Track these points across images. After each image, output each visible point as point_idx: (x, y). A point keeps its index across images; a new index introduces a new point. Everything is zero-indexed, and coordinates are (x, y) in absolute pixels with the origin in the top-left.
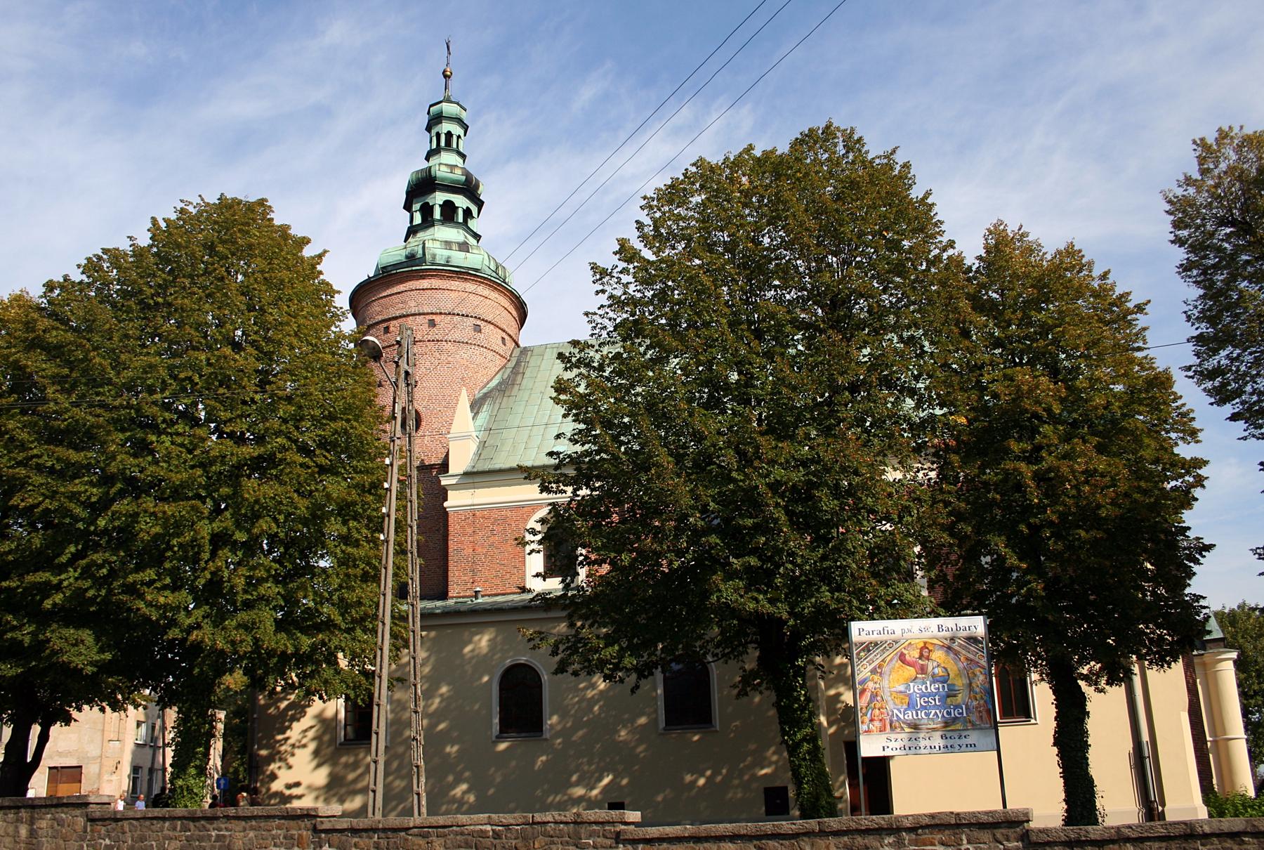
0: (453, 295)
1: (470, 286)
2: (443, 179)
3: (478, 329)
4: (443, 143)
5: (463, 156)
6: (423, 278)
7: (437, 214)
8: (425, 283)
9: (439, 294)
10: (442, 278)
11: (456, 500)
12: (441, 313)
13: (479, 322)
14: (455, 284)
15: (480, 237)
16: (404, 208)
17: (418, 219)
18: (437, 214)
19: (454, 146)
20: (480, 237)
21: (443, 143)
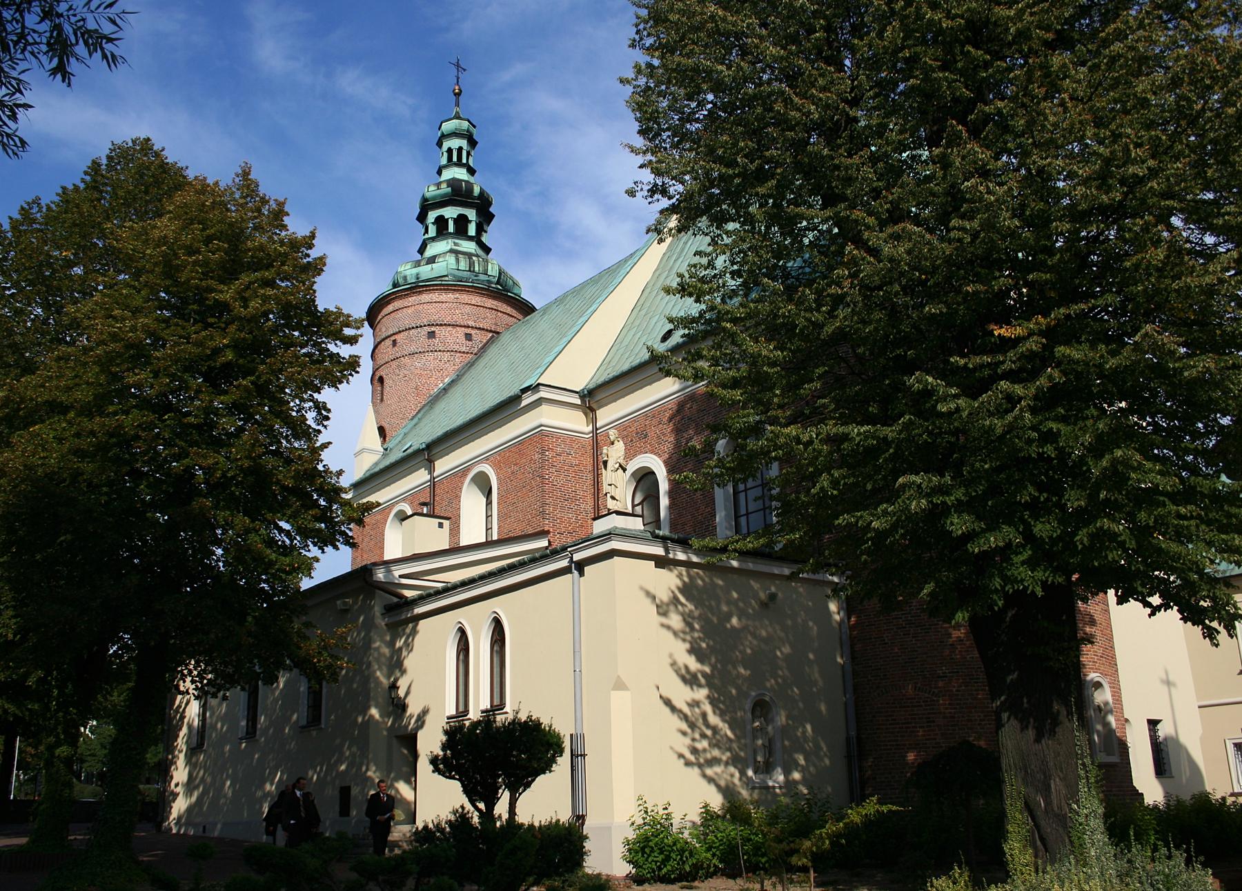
0: (410, 311)
1: (426, 297)
2: (434, 197)
3: (432, 335)
4: (455, 159)
5: (471, 171)
6: (388, 303)
7: (451, 228)
8: (390, 308)
9: (399, 314)
10: (400, 297)
11: (495, 537)
12: (400, 332)
13: (469, 331)
14: (412, 300)
15: (490, 250)
16: (418, 219)
17: (432, 231)
18: (451, 228)
19: (464, 161)
20: (490, 250)
21: (455, 159)
